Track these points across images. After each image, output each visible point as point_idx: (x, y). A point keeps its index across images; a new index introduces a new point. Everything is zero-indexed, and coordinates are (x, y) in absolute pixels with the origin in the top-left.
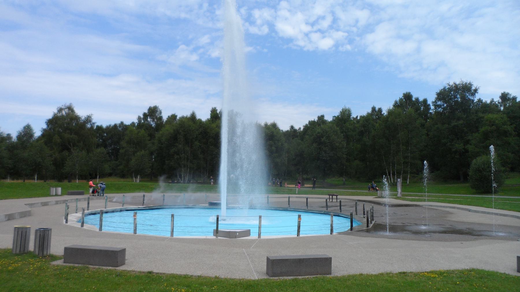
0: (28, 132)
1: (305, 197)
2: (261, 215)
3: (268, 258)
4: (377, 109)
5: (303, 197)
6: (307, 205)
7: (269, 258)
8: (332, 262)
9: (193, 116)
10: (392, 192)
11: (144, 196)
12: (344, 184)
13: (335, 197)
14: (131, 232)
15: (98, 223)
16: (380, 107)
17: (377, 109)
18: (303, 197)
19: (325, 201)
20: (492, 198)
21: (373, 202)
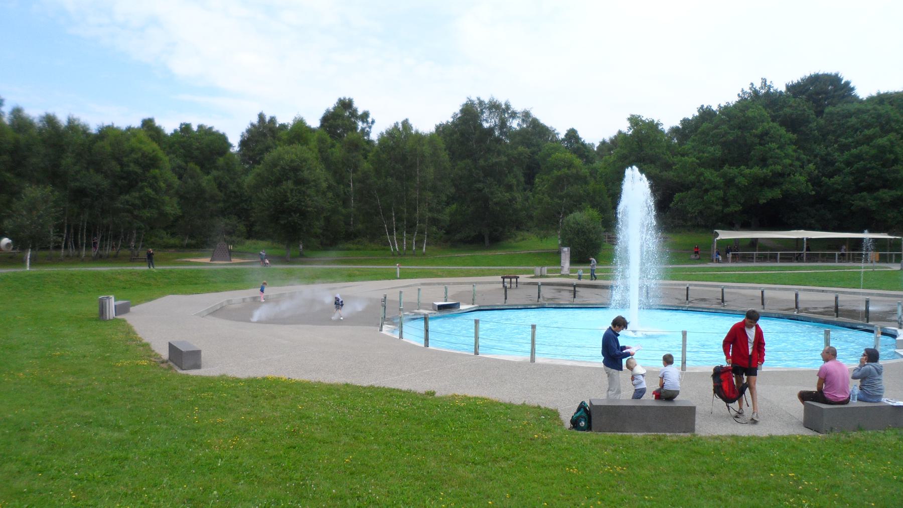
0: (568, 203)
1: (760, 288)
2: (684, 330)
3: (173, 346)
4: (267, 119)
5: (717, 286)
6: (763, 304)
7: (173, 344)
8: (696, 422)
9: (620, 132)
10: (836, 259)
11: (401, 292)
12: (302, 255)
13: (509, 280)
14: (528, 357)
15: (688, 355)
16: (273, 115)
17: (267, 119)
18: (717, 286)
19: (834, 299)
20: (753, 254)
21: (592, 285)
